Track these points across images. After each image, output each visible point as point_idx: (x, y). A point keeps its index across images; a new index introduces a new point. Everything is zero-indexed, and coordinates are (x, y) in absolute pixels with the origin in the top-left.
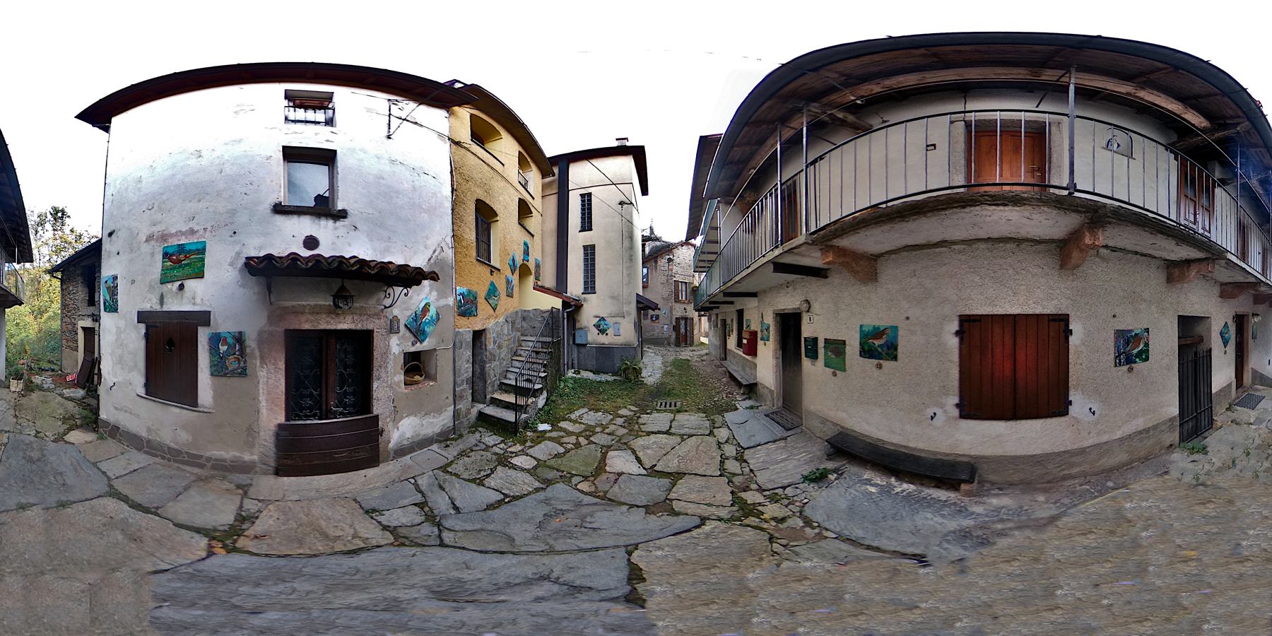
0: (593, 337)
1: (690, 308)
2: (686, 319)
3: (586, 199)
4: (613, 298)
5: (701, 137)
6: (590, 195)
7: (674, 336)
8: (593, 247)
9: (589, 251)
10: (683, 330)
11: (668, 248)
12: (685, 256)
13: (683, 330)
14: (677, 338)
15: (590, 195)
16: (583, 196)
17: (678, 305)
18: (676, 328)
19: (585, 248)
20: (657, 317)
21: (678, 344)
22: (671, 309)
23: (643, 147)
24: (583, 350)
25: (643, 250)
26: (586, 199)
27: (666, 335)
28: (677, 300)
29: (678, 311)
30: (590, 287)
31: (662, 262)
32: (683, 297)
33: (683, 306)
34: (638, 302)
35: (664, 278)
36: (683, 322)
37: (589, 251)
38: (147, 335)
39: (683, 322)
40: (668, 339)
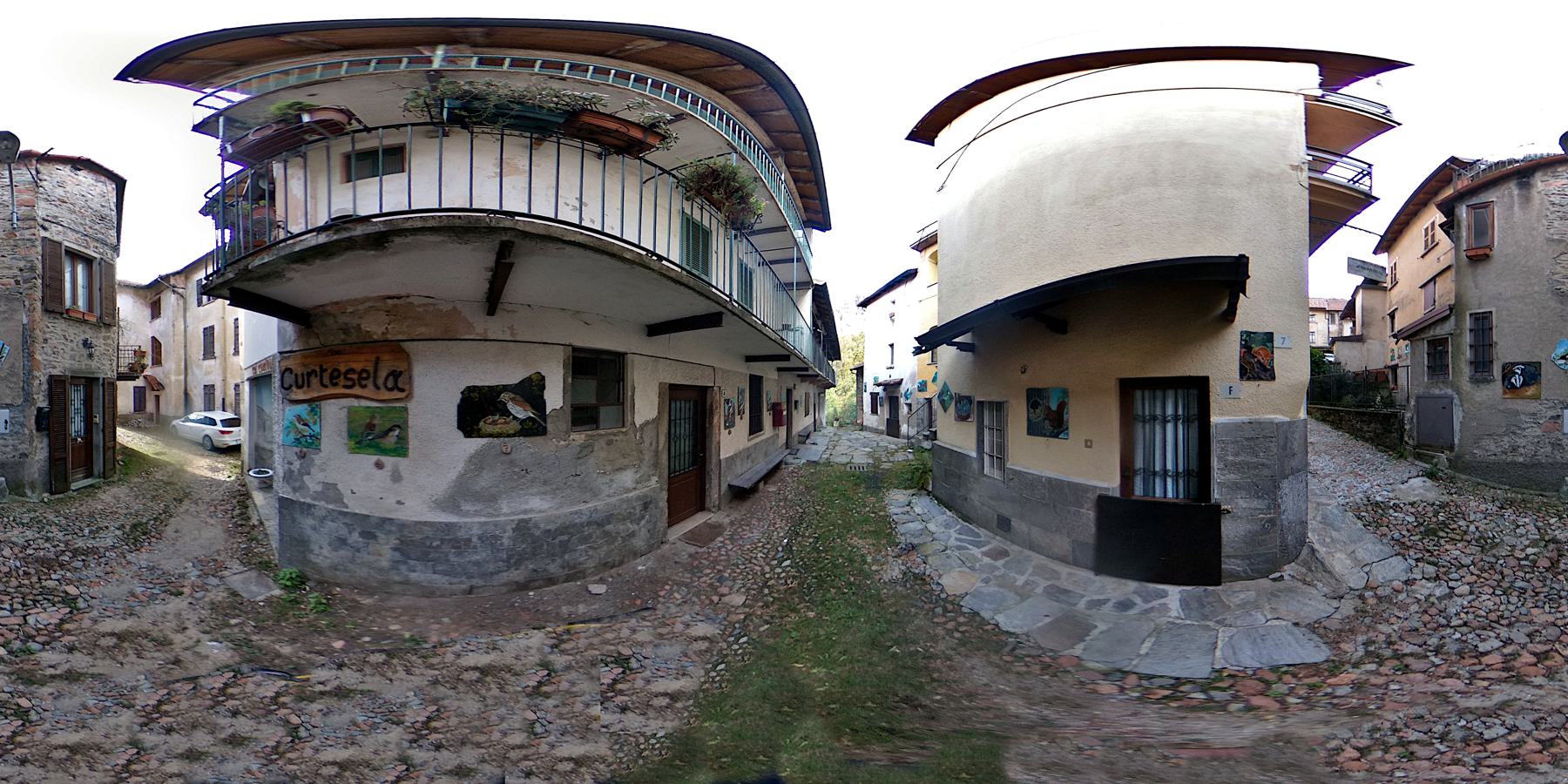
7: (39, 452)
10: (76, 426)
13: (76, 426)
17: (60, 326)
18: (50, 422)
36: (76, 398)
39: (76, 398)
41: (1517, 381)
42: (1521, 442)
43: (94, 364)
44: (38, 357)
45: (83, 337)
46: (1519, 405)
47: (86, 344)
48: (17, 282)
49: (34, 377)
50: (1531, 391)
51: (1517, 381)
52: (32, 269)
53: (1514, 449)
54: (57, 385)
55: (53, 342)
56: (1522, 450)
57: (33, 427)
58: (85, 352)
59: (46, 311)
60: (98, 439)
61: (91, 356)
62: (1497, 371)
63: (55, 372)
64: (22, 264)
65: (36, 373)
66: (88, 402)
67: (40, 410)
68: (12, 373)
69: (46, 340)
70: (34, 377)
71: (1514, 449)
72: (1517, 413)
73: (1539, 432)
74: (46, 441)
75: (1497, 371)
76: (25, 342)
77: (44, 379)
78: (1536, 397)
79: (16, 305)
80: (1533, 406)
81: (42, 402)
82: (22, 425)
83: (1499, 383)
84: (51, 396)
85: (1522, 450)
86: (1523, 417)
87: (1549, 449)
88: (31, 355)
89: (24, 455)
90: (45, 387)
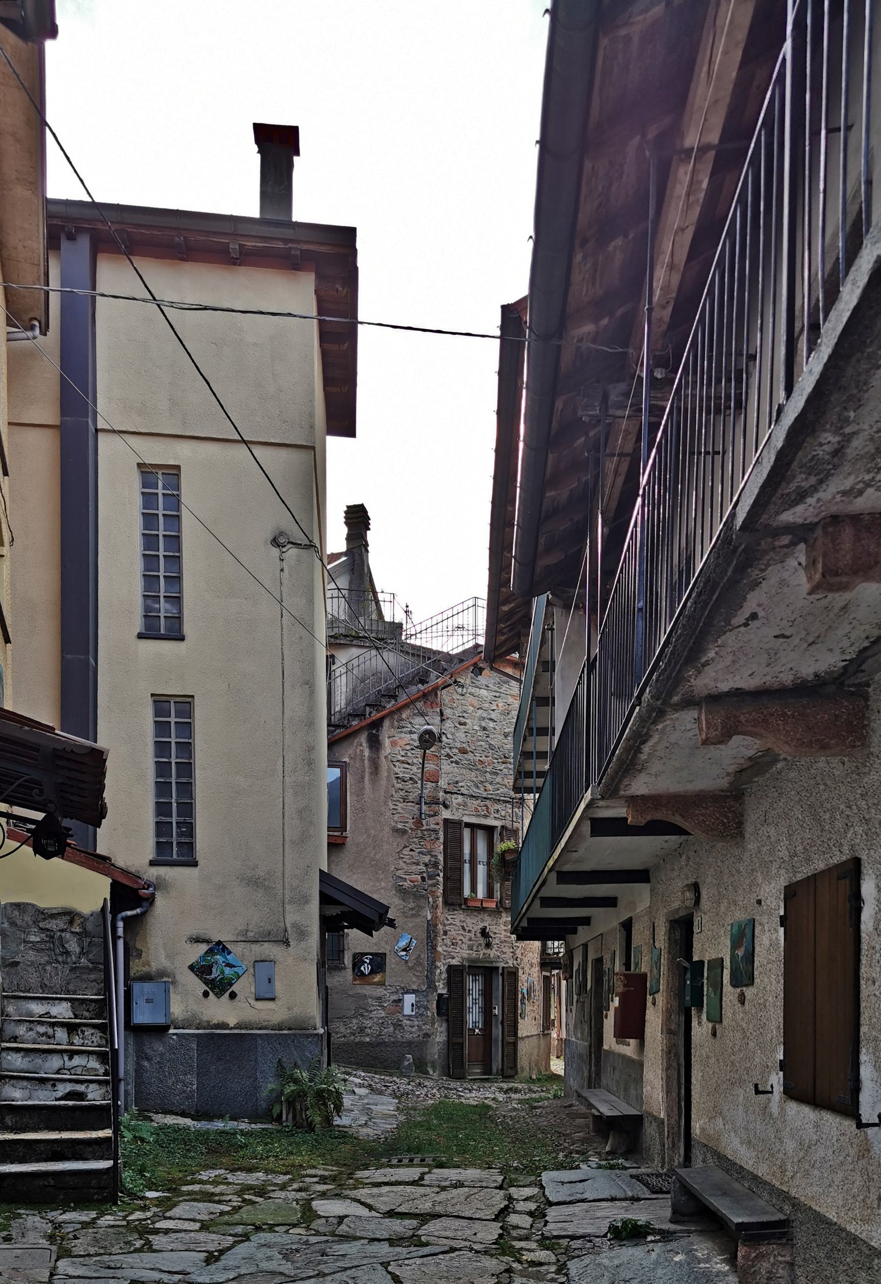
0: (188, 1003)
1: (501, 927)
2: (487, 972)
3: (161, 486)
4: (254, 882)
5: (362, 505)
6: (173, 472)
7: (440, 1035)
8: (186, 704)
9: (173, 716)
10: (473, 1017)
11: (430, 675)
12: (490, 706)
13: (473, 1017)
14: (454, 1046)
15: (173, 472)
16: (147, 471)
17: (458, 917)
18: (450, 1008)
19: (160, 703)
20: (379, 962)
21: (454, 1067)
22: (431, 933)
23: (350, 233)
24: (158, 1047)
25: (823, 271)
26: (161, 486)
27: (411, 1033)
28: (454, 899)
29: (457, 940)
30: (176, 841)
31: (399, 742)
32: (478, 884)
33: (475, 924)
34: (325, 899)
35: (406, 812)
36: (474, 987)
37: (173, 716)
38: (111, 884)
39: (474, 987)
40: (418, 1046)
41: (366, 969)
42: (368, 1023)
43: (493, 953)
44: (439, 949)
45: (481, 925)
46: (367, 990)
47: (484, 933)
48: (423, 879)
49: (437, 967)
50: (377, 978)
51: (366, 969)
52: (436, 865)
53: (362, 1030)
54: (456, 974)
55: (453, 933)
56: (368, 1031)
57: (435, 1011)
58: (482, 941)
59: (446, 903)
60: (497, 1031)
61: (488, 945)
62: (348, 960)
63: (454, 962)
64: (427, 859)
65: (439, 964)
66: (487, 994)
67: (440, 996)
68: (418, 963)
69: (445, 933)
70: (437, 967)
71: (362, 1030)
72: (365, 997)
73: (383, 1014)
74: (445, 1025)
75: (348, 960)
76: (429, 937)
77: (443, 969)
78: (382, 984)
79: (422, 902)
80: (380, 991)
81: (442, 989)
82: (426, 1008)
83: (349, 971)
84: (449, 983)
85: (368, 1031)
86: (370, 1000)
87: (392, 1029)
88: (434, 948)
89: (427, 1035)
90: (444, 976)
